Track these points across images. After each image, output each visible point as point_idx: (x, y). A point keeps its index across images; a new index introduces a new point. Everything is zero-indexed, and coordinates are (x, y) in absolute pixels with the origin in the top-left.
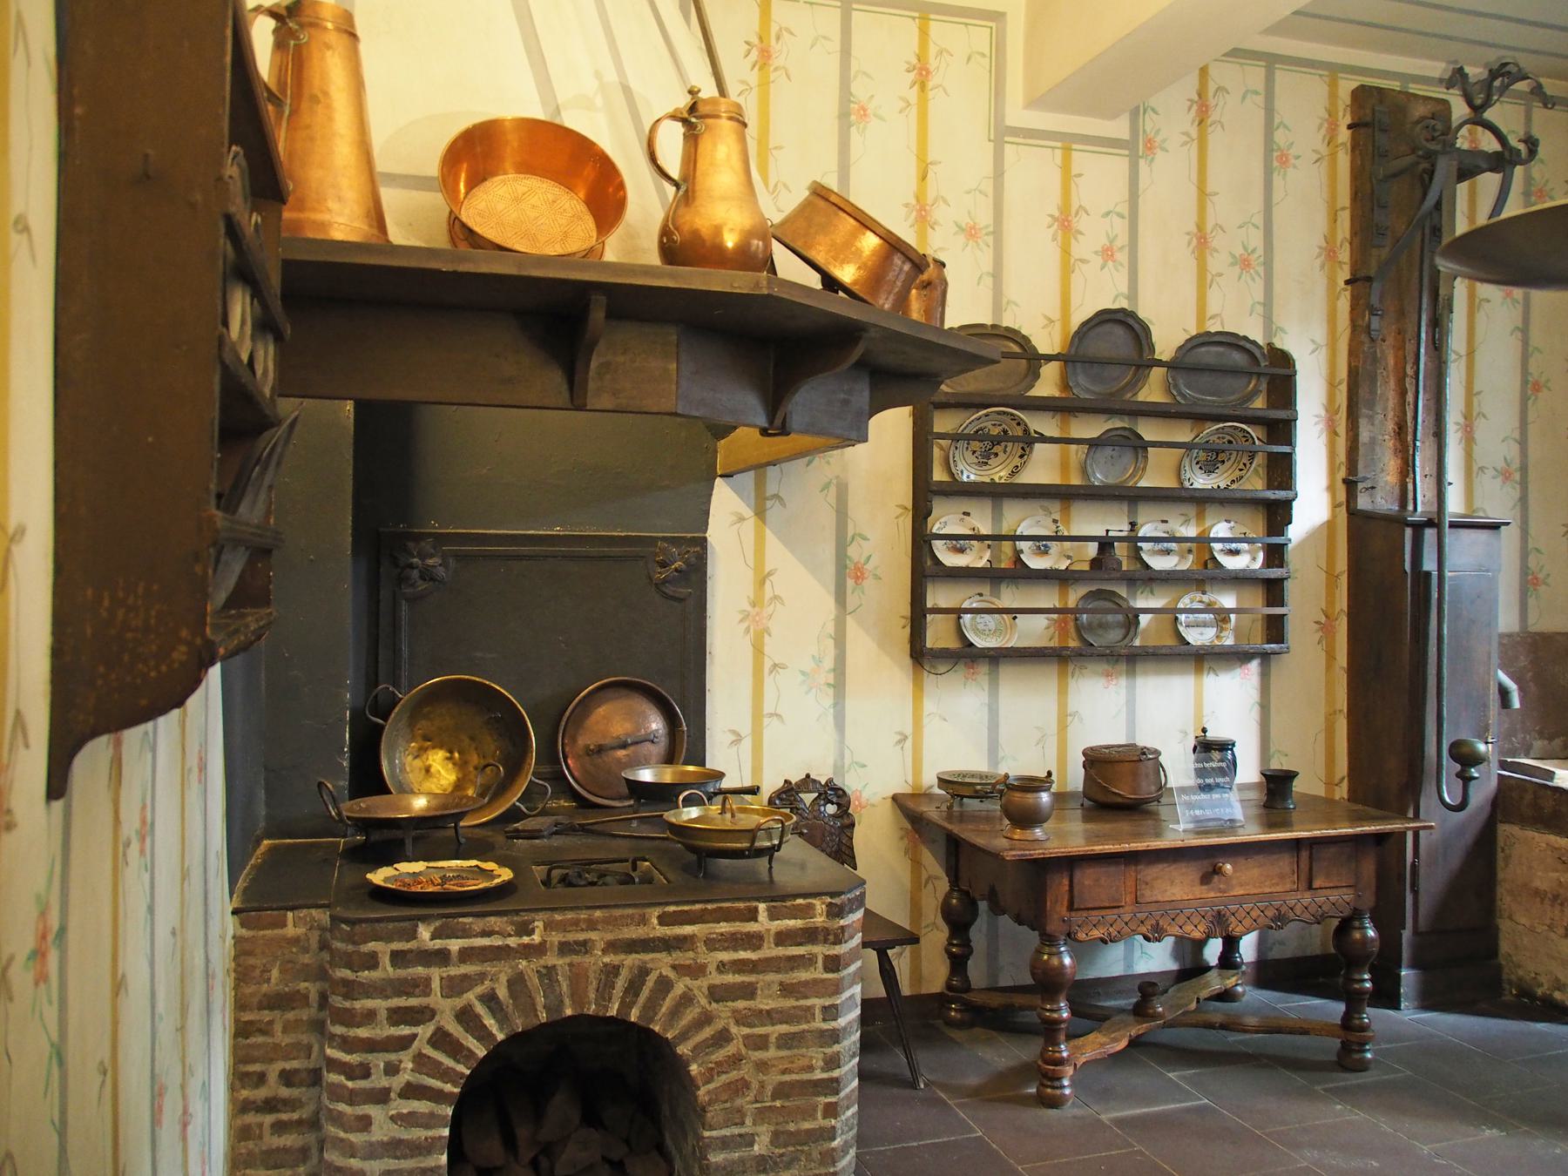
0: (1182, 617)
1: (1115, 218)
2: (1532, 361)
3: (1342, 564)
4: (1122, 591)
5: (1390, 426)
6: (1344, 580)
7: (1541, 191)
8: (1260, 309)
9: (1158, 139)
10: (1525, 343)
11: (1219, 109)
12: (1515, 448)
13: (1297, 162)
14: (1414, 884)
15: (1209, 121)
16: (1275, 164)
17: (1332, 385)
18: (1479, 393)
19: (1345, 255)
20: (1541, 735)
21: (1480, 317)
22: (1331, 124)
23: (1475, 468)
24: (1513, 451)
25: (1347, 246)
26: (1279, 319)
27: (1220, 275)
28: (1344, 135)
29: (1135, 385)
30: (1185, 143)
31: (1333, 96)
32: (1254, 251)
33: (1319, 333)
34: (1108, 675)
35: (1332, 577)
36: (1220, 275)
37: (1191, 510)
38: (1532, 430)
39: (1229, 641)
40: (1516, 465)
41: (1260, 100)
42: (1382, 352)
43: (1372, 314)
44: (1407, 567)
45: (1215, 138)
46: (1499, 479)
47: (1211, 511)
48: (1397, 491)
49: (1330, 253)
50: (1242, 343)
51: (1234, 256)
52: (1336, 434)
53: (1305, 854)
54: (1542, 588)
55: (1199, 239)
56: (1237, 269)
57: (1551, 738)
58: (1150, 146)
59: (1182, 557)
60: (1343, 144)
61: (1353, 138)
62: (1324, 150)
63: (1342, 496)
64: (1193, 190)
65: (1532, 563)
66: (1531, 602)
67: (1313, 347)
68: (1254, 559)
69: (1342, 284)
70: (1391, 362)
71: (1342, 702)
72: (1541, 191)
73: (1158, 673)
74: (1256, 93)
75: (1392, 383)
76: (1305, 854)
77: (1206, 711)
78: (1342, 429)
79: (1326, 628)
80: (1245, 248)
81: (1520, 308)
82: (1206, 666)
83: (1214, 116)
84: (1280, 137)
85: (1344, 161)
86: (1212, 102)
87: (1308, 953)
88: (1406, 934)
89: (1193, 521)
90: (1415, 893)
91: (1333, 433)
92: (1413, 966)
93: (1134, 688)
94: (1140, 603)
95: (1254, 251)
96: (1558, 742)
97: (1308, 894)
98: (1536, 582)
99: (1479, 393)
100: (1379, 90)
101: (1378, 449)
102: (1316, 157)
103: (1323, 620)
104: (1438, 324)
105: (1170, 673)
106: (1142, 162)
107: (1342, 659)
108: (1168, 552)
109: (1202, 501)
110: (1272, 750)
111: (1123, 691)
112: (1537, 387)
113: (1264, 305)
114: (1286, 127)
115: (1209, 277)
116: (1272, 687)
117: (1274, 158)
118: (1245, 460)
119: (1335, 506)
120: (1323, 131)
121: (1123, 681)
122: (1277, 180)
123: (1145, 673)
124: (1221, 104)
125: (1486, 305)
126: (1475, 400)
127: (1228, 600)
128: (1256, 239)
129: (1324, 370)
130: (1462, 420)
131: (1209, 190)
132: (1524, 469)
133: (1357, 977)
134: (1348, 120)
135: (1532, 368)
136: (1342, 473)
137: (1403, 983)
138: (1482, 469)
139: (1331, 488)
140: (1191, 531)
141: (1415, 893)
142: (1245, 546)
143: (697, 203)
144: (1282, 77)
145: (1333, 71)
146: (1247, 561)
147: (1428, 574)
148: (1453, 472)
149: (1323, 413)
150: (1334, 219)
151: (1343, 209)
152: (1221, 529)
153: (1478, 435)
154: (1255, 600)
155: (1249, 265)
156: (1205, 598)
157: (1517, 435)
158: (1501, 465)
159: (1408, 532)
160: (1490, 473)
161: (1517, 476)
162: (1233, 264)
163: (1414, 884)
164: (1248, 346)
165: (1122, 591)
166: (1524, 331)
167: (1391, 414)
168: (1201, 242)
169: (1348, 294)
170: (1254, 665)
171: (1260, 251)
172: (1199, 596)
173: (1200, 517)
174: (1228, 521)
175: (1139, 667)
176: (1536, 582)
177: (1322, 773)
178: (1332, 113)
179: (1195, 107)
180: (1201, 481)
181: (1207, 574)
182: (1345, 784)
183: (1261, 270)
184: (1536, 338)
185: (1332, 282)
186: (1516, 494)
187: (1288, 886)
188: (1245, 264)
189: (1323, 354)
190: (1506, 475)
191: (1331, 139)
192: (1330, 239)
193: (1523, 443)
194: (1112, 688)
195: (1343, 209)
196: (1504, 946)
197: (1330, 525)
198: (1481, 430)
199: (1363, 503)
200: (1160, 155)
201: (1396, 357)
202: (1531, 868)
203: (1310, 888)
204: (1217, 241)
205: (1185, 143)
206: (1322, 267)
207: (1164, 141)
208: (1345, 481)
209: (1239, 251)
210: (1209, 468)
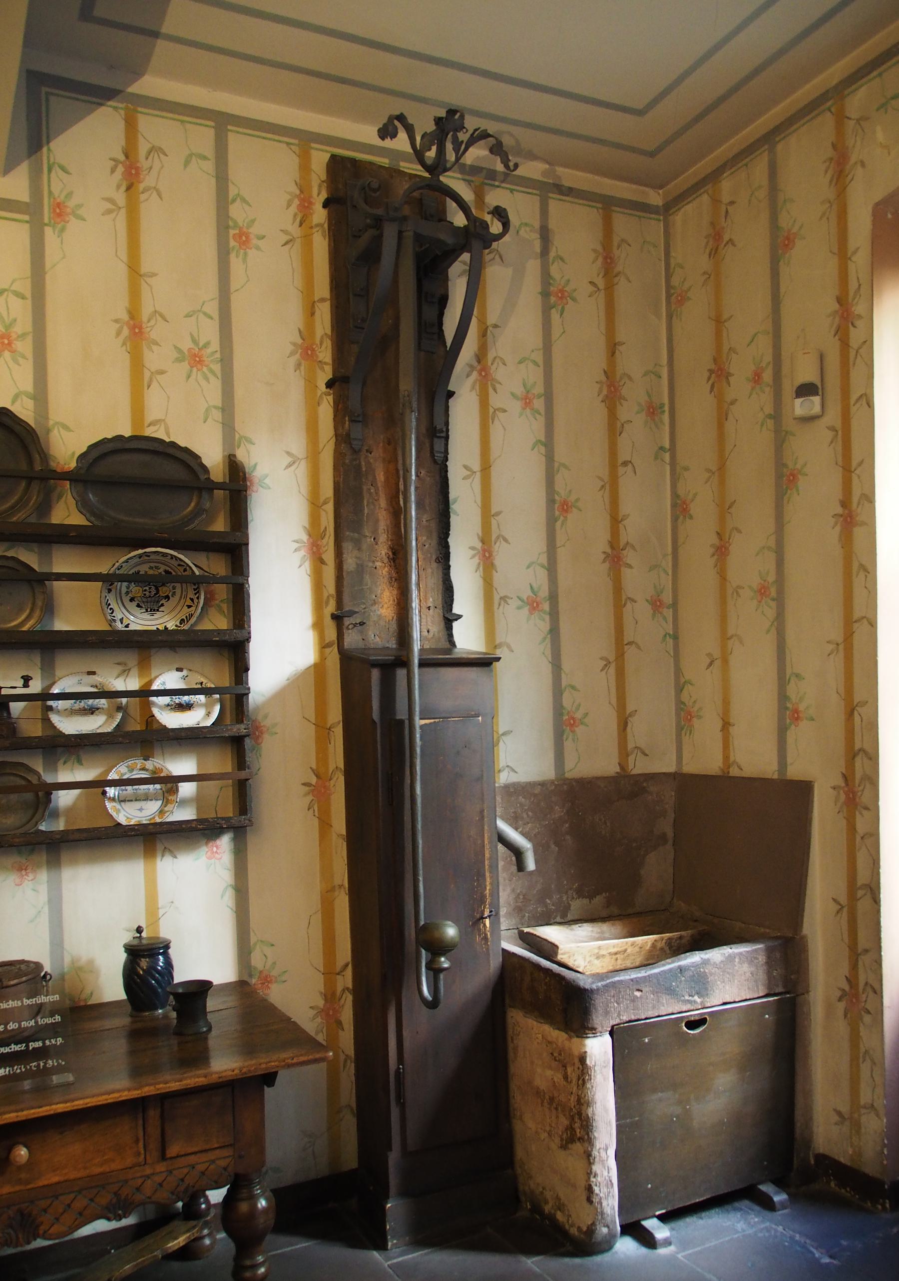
0: (111, 791)
1: (12, 299)
2: (558, 478)
3: (335, 714)
4: (37, 764)
5: (383, 550)
6: (339, 732)
7: (562, 291)
8: (217, 415)
9: (71, 204)
10: (550, 458)
11: (154, 172)
12: (543, 575)
13: (260, 243)
14: (400, 1096)
15: (141, 186)
16: (232, 243)
17: (315, 505)
18: (498, 514)
19: (326, 354)
20: (580, 893)
21: (496, 432)
22: (303, 201)
23: (496, 599)
24: (541, 578)
25: (328, 343)
26: (242, 427)
27: (162, 372)
28: (320, 215)
29: (45, 507)
30: (109, 212)
31: (305, 167)
32: (207, 345)
33: (297, 444)
34: (21, 869)
35: (322, 731)
36: (162, 372)
37: (131, 658)
38: (562, 554)
39: (186, 814)
40: (544, 592)
41: (209, 166)
42: (368, 464)
43: (352, 421)
44: (376, 715)
45: (152, 211)
46: (526, 610)
47: (157, 658)
48: (394, 626)
49: (307, 352)
50: (171, 451)
51: (179, 351)
52: (322, 562)
53: (153, 1114)
54: (579, 730)
55: (132, 328)
56: (185, 365)
57: (591, 897)
58: (60, 211)
59: (111, 717)
60: (321, 225)
61: (330, 218)
62: (295, 230)
63: (331, 634)
64: (122, 270)
65: (567, 701)
66: (568, 745)
67: (290, 459)
68: (208, 714)
69: (323, 387)
70: (381, 477)
71: (341, 874)
72: (562, 291)
73: (92, 860)
74: (205, 158)
75: (383, 502)
76: (153, 1114)
77: (161, 902)
78: (329, 556)
79: (318, 791)
80: (194, 341)
81: (542, 419)
82: (159, 847)
83: (148, 181)
84: (236, 212)
85: (321, 245)
86: (143, 163)
87: (281, 1186)
88: (394, 1157)
89: (135, 671)
90: (402, 1106)
91: (318, 561)
92: (404, 1193)
93: (154, 871)
94: (64, 776)
95: (207, 345)
96: (599, 900)
97: (161, 1167)
98: (573, 723)
99: (498, 514)
100: (354, 161)
101: (367, 578)
102: (286, 238)
103: (314, 780)
104: (436, 435)
105: (111, 858)
106: (48, 231)
107: (339, 824)
108: (92, 711)
109: (144, 646)
110: (253, 939)
111: (43, 889)
112: (566, 507)
113: (223, 410)
114: (244, 200)
115: (147, 375)
116: (250, 866)
117: (230, 238)
118: (191, 594)
119: (323, 646)
120: (293, 208)
121: (43, 876)
122: (236, 264)
123: (74, 862)
124: (157, 165)
125: (500, 415)
126: (494, 522)
127: (182, 765)
128: (210, 333)
129: (305, 489)
130: (479, 545)
131: (143, 270)
132: (553, 598)
133: (248, 1263)
134: (324, 196)
135: (559, 486)
136: (331, 608)
137: (389, 1217)
138: (504, 599)
139: (318, 625)
140: (133, 684)
141: (402, 1106)
142: (202, 698)
143: (224, 457)
144: (237, 142)
145: (305, 140)
146: (200, 716)
147: (401, 722)
148: (466, 602)
149: (305, 538)
150: (310, 312)
151: (322, 300)
152: (170, 679)
153: (498, 561)
154: (220, 762)
155: (201, 362)
156: (149, 765)
157: (544, 560)
158: (527, 593)
159: (375, 674)
160: (514, 603)
161: (546, 606)
162: (178, 360)
163: (400, 1096)
164: (178, 454)
165: (37, 764)
166: (548, 444)
167: (383, 538)
168: (136, 331)
169: (331, 398)
170: (225, 842)
171: (215, 346)
172: (139, 763)
173: (144, 665)
174: (179, 670)
175: (64, 856)
176: (573, 723)
177: (319, 963)
178: (303, 189)
179: (120, 169)
180: (139, 621)
181: (152, 738)
182: (349, 972)
183: (217, 368)
184: (561, 453)
185: (310, 383)
186: (545, 626)
187: (130, 1161)
188: (196, 360)
189: (302, 470)
190: (533, 605)
191: (303, 221)
192: (307, 333)
193: (552, 568)
194: (28, 884)
195: (322, 300)
196: (520, 1153)
197: (318, 669)
198: (502, 555)
199: (352, 639)
200: (73, 224)
201: (387, 472)
202: (532, 1063)
203: (163, 1157)
204: (156, 331)
205: (109, 212)
206: (298, 366)
207: (80, 206)
208: (334, 617)
209: (186, 345)
210: (152, 605)
